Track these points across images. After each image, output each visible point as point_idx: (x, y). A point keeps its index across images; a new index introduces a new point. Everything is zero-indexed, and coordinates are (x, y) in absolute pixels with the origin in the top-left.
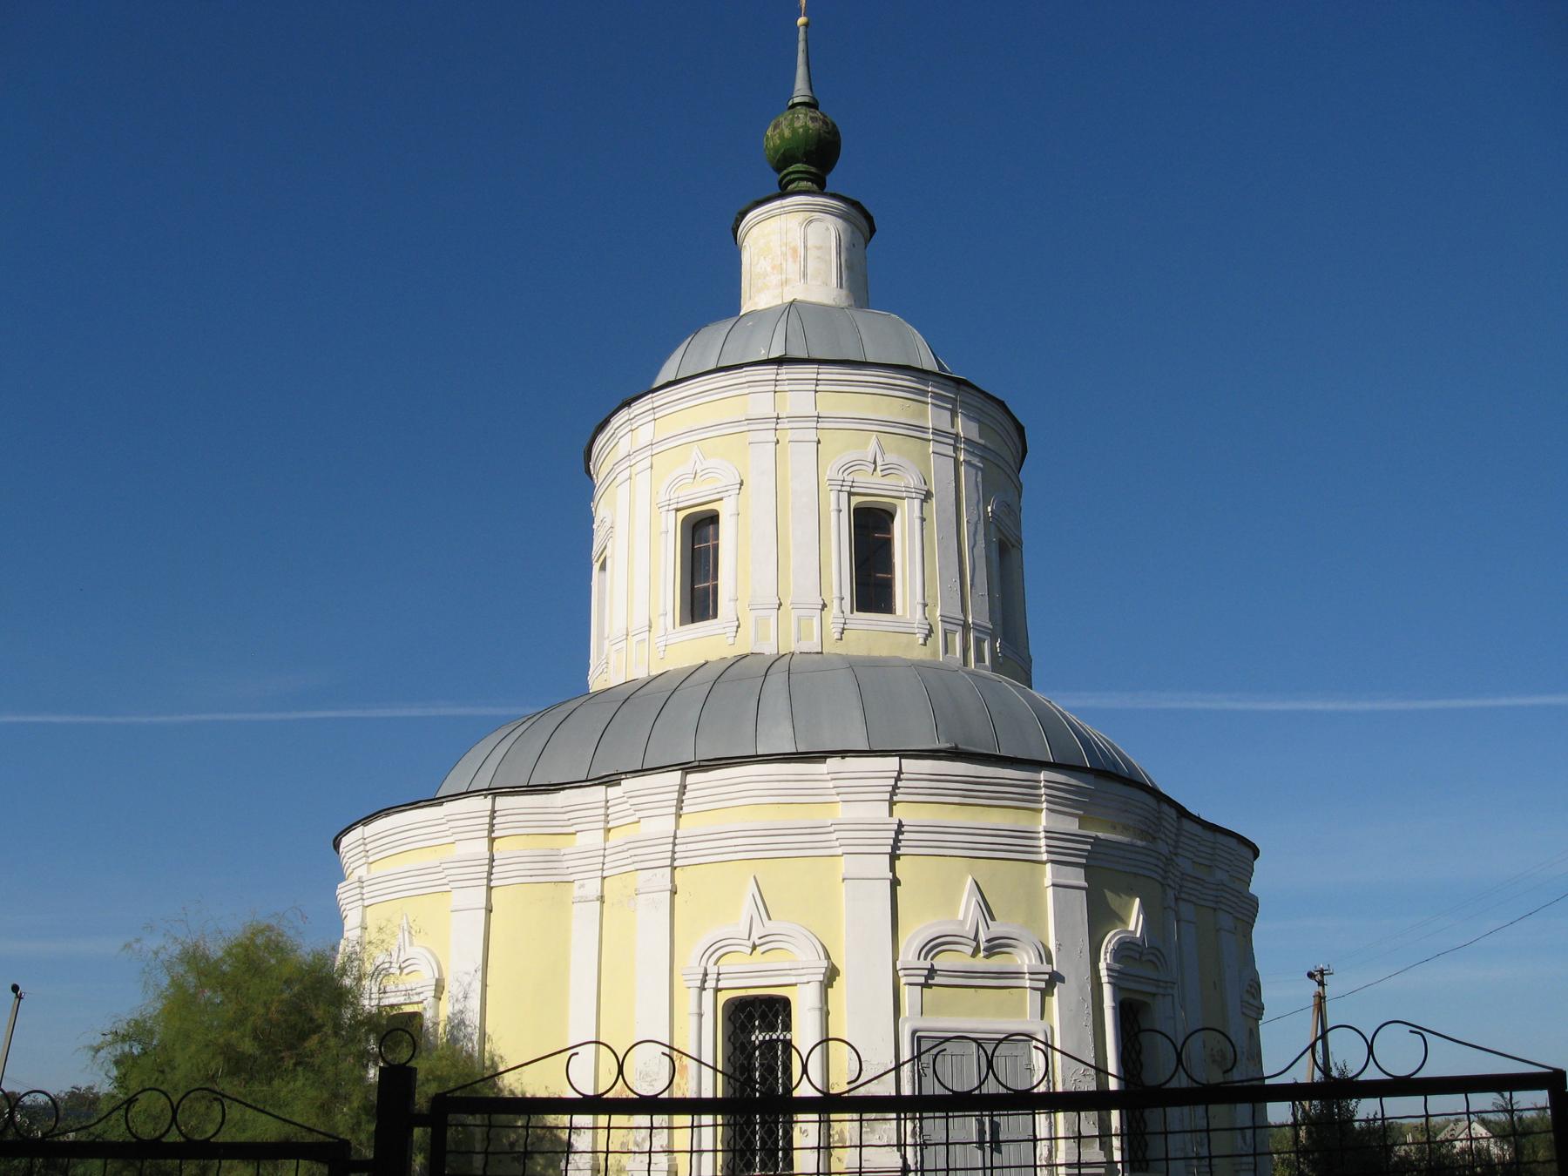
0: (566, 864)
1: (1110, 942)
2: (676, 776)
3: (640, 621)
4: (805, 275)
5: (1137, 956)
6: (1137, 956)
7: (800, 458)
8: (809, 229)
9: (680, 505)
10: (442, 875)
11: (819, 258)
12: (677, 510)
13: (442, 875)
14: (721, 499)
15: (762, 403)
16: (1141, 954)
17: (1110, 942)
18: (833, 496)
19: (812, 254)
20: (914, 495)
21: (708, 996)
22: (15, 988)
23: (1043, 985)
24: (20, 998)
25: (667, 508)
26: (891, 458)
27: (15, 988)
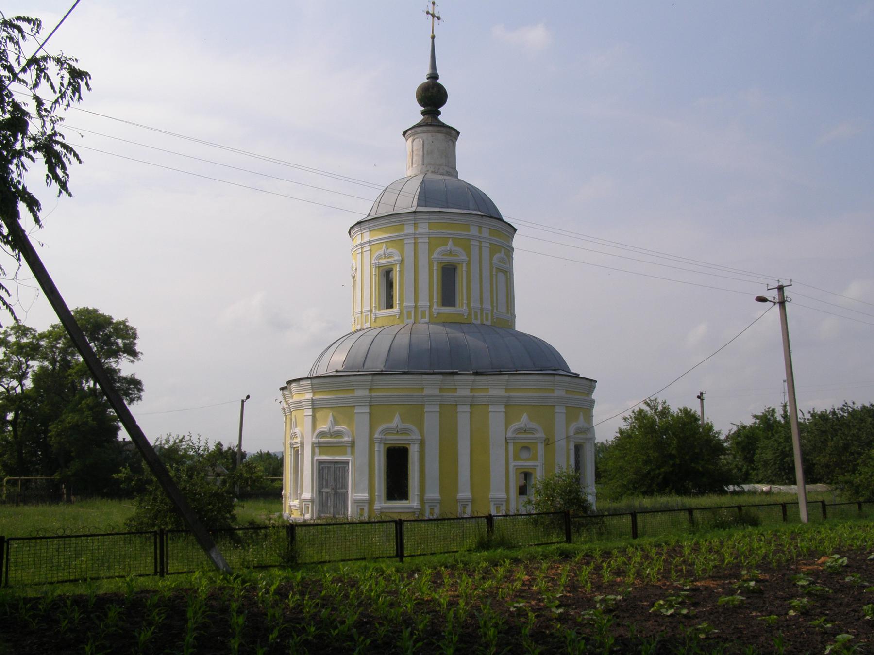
16: (397, 431)
18: (374, 269)
19: (415, 152)
26: (390, 250)
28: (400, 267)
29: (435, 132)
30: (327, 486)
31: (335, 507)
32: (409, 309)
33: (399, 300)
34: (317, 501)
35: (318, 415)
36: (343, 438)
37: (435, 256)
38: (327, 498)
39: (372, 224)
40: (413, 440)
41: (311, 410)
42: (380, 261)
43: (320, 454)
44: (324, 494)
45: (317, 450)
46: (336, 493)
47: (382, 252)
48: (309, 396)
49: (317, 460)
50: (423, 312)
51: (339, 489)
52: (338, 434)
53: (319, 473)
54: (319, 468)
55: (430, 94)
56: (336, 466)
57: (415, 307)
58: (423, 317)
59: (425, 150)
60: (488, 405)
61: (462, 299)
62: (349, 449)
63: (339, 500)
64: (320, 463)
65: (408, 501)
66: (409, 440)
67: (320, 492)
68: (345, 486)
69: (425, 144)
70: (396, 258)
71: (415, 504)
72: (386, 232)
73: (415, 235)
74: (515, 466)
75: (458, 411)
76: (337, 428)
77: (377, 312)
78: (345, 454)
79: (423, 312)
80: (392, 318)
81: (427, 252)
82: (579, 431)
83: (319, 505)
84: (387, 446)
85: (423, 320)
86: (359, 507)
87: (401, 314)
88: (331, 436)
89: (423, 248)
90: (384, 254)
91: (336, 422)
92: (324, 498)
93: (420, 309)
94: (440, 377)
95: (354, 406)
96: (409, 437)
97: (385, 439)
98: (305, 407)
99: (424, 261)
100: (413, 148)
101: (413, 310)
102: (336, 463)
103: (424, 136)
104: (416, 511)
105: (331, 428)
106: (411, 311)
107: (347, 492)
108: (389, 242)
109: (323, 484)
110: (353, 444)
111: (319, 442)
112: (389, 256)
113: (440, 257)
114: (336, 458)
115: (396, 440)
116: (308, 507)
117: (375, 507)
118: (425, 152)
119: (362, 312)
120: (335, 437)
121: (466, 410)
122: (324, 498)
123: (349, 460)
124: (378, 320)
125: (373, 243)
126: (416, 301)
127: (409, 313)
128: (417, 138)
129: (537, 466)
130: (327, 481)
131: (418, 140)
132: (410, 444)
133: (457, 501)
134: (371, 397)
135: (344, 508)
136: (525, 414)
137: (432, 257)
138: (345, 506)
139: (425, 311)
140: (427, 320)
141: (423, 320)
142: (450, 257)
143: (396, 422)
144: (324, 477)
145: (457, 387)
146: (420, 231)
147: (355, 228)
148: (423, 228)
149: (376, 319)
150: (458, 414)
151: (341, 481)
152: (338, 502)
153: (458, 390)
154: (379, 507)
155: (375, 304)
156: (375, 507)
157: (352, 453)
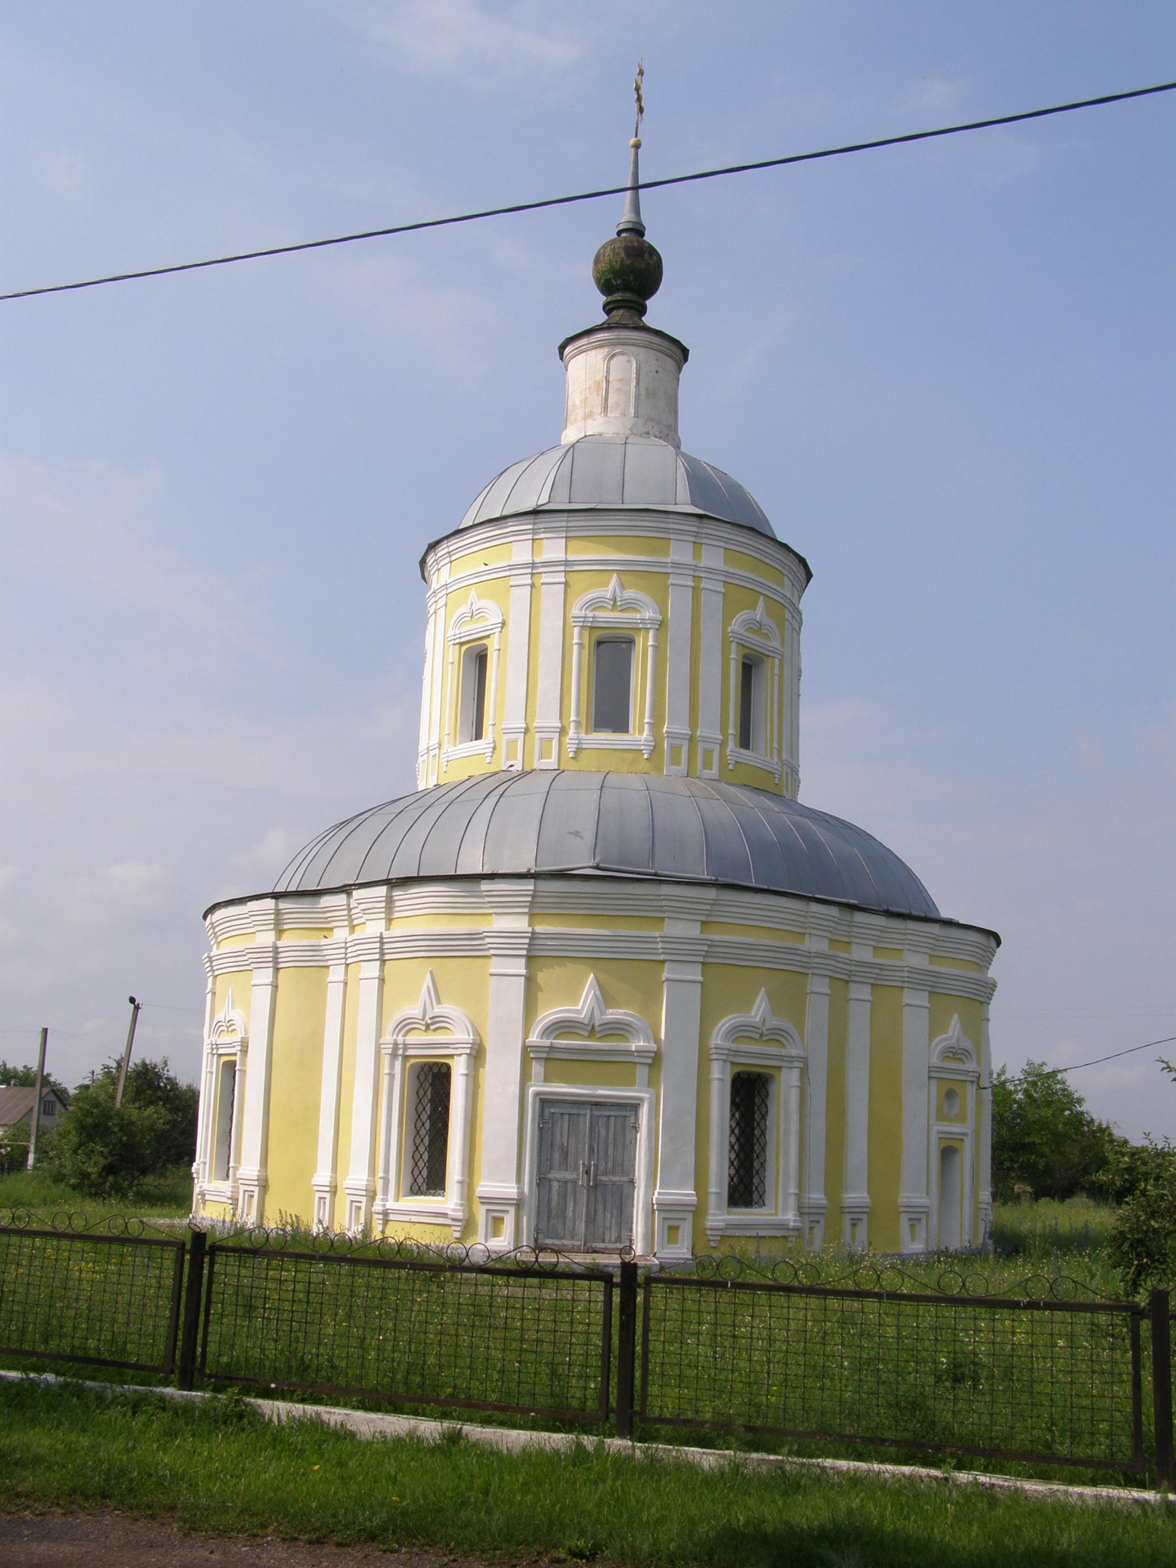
0: (325, 953)
1: (723, 1025)
2: (382, 890)
3: (434, 741)
4: (605, 408)
5: (757, 1036)
6: (757, 1036)
7: (551, 599)
8: (612, 362)
9: (463, 640)
10: (245, 958)
11: (618, 389)
12: (461, 644)
13: (245, 958)
14: (488, 636)
15: (521, 552)
16: (761, 1035)
17: (725, 1023)
18: (576, 630)
19: (613, 386)
20: (649, 626)
21: (398, 1064)
22: (132, 1000)
23: (650, 1061)
24: (137, 1008)
25: (452, 642)
26: (630, 593)
27: (132, 1000)
28: (656, 638)
29: (660, 351)
30: (564, 1164)
31: (591, 1220)
32: (677, 742)
33: (652, 716)
34: (531, 1205)
35: (542, 977)
36: (627, 1039)
37: (734, 626)
38: (563, 1196)
39: (577, 521)
40: (791, 1059)
41: (523, 961)
42: (599, 614)
43: (547, 1079)
44: (555, 1184)
45: (537, 1068)
46: (595, 1187)
47: (609, 595)
48: (520, 924)
49: (537, 1094)
50: (708, 753)
51: (605, 1174)
52: (617, 1030)
53: (541, 1129)
54: (542, 1115)
55: (643, 266)
56: (596, 1113)
57: (692, 739)
58: (707, 765)
59: (642, 384)
60: (902, 988)
61: (772, 740)
62: (642, 1073)
63: (596, 1201)
64: (545, 1102)
65: (763, 1210)
66: (781, 1057)
67: (542, 1181)
68: (625, 1166)
69: (643, 372)
70: (648, 615)
71: (453, 1206)
72: (620, 550)
73: (533, 568)
74: (939, 1132)
75: (852, 995)
76: (613, 1014)
77: (583, 736)
78: (630, 1082)
79: (708, 753)
80: (630, 756)
81: (720, 616)
82: (953, 1053)
83: (539, 1214)
84: (738, 1069)
85: (707, 773)
86: (354, 1204)
87: (656, 750)
88: (592, 1032)
89: (712, 605)
90: (615, 600)
91: (606, 998)
92: (555, 1198)
93: (700, 747)
94: (834, 911)
95: (663, 962)
96: (783, 1052)
97: (737, 1052)
98: (492, 952)
99: (711, 636)
100: (608, 372)
101: (685, 744)
102: (597, 1104)
103: (643, 353)
104: (791, 1233)
105: (596, 1012)
106: (680, 747)
107: (632, 1182)
108: (628, 572)
109: (551, 1159)
110: (655, 1060)
111: (552, 1048)
112: (629, 606)
113: (742, 631)
114: (601, 1092)
115: (755, 1054)
116: (359, 1208)
117: (709, 1224)
118: (643, 392)
119: (527, 731)
120: (601, 1038)
121: (862, 997)
122: (555, 1198)
123: (641, 1099)
124: (583, 755)
125: (576, 568)
126: (693, 724)
127: (675, 750)
128: (623, 354)
129: (965, 1134)
130: (565, 1152)
131: (625, 358)
132: (780, 1068)
133: (842, 1210)
134: (534, 936)
135: (619, 1226)
136: (956, 1016)
137: (729, 630)
138: (624, 1221)
139: (712, 751)
140: (714, 772)
141: (707, 773)
142: (758, 638)
143: (758, 1011)
144: (558, 1139)
145: (853, 940)
146: (704, 562)
147: (511, 522)
148: (713, 558)
149: (578, 751)
150: (852, 1004)
151: (610, 1153)
152: (600, 1207)
153: (854, 946)
154: (722, 1224)
155: (578, 714)
156: (709, 1224)
157: (652, 1082)
